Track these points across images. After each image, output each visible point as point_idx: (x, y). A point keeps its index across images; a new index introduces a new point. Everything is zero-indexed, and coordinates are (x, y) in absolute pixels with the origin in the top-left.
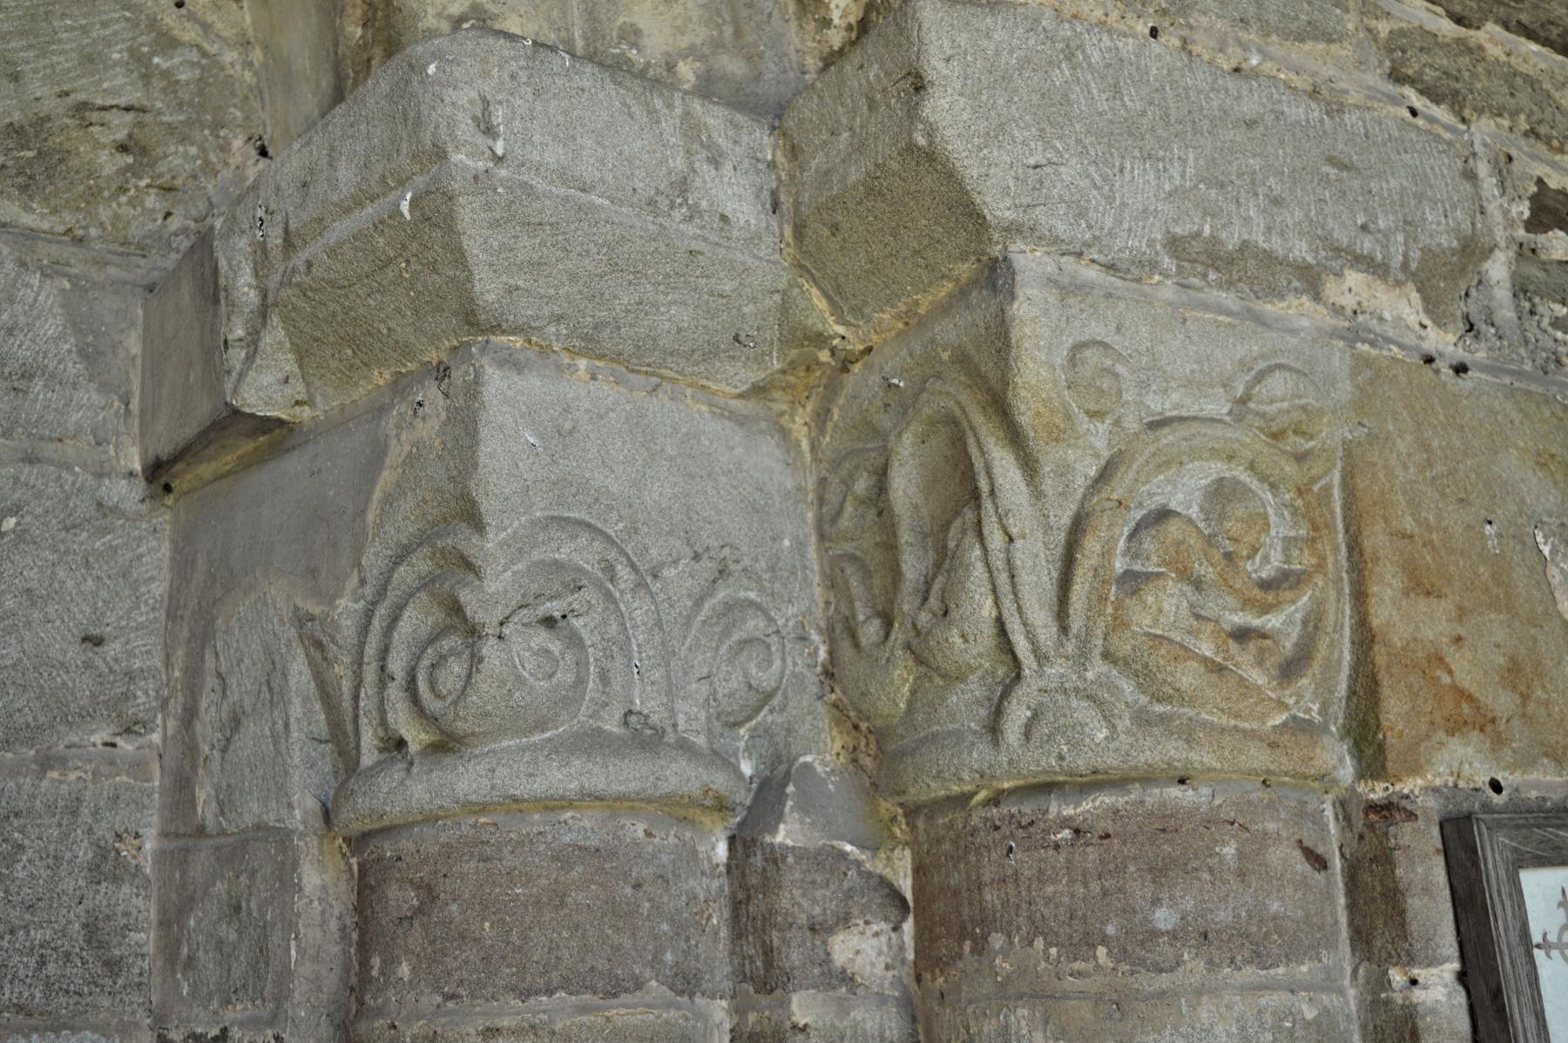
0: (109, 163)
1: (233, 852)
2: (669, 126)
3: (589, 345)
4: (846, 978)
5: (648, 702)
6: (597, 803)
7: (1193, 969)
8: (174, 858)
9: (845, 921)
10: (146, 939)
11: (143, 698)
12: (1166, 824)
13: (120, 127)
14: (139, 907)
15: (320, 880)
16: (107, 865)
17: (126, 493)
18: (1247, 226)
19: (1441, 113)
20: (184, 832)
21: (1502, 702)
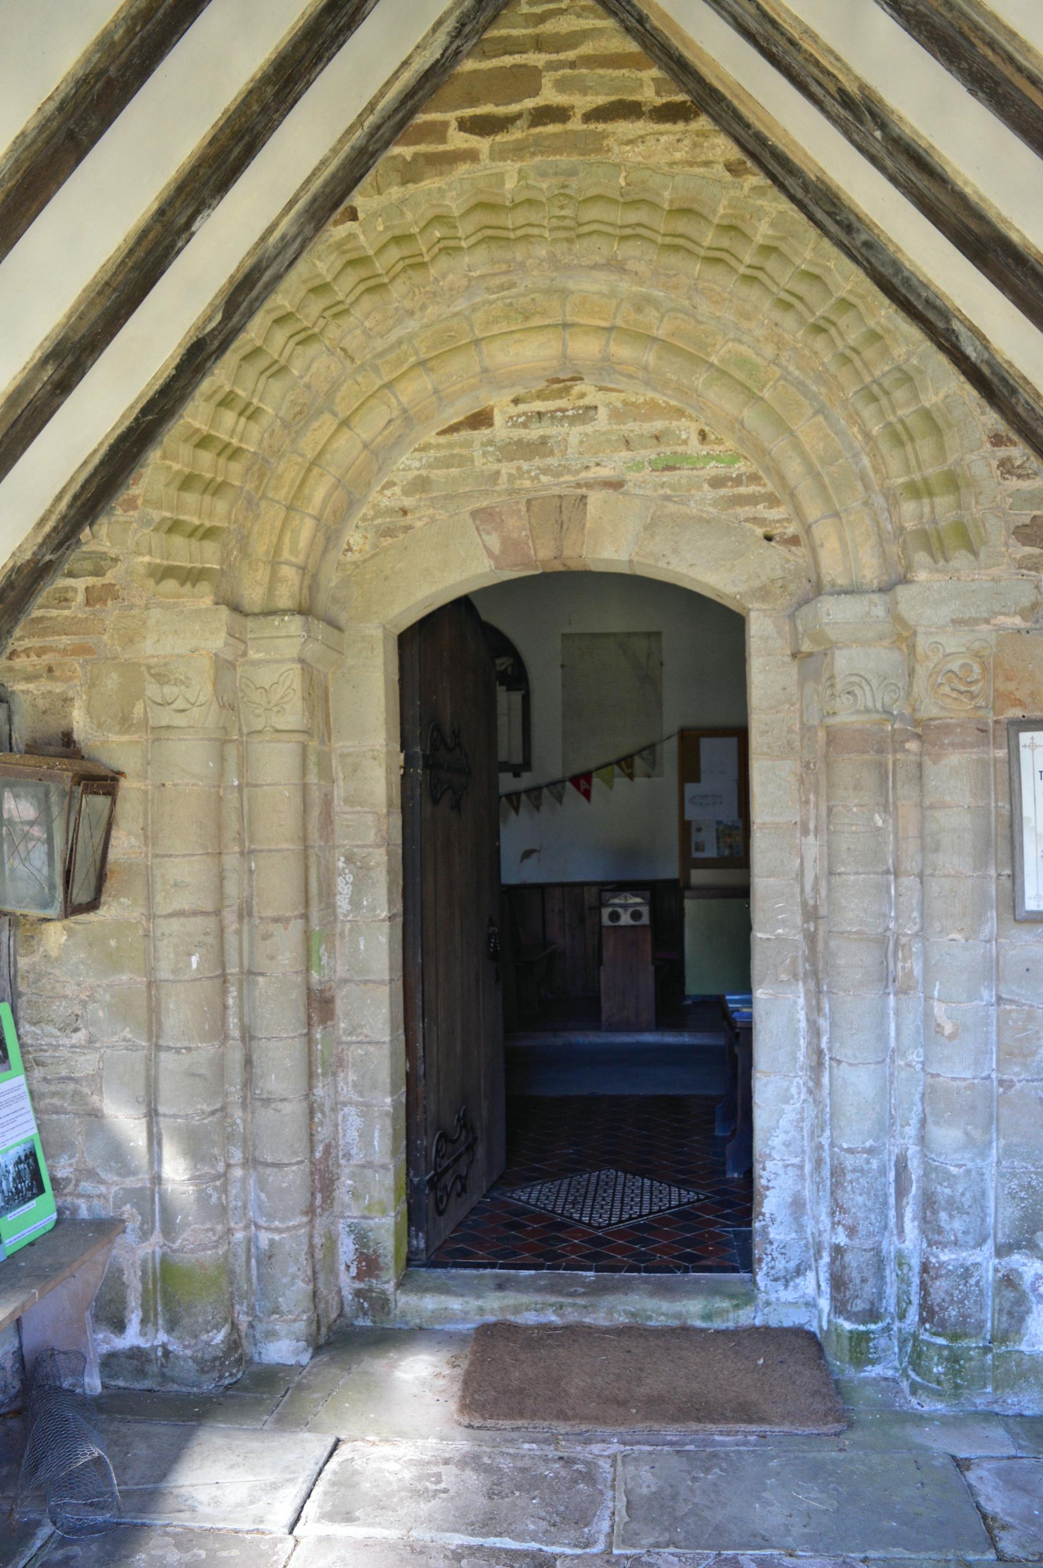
0: (779, 591)
1: (809, 729)
2: (865, 603)
3: (855, 641)
4: (908, 751)
5: (870, 704)
6: (59, 868)
7: (950, 749)
8: (801, 729)
9: (908, 740)
10: (798, 744)
11: (794, 699)
12: (947, 726)
13: (780, 583)
14: (796, 737)
15: (821, 735)
16: (790, 731)
17: (788, 659)
18: (973, 613)
19: (1033, 573)
20: (802, 724)
21: (1028, 700)
